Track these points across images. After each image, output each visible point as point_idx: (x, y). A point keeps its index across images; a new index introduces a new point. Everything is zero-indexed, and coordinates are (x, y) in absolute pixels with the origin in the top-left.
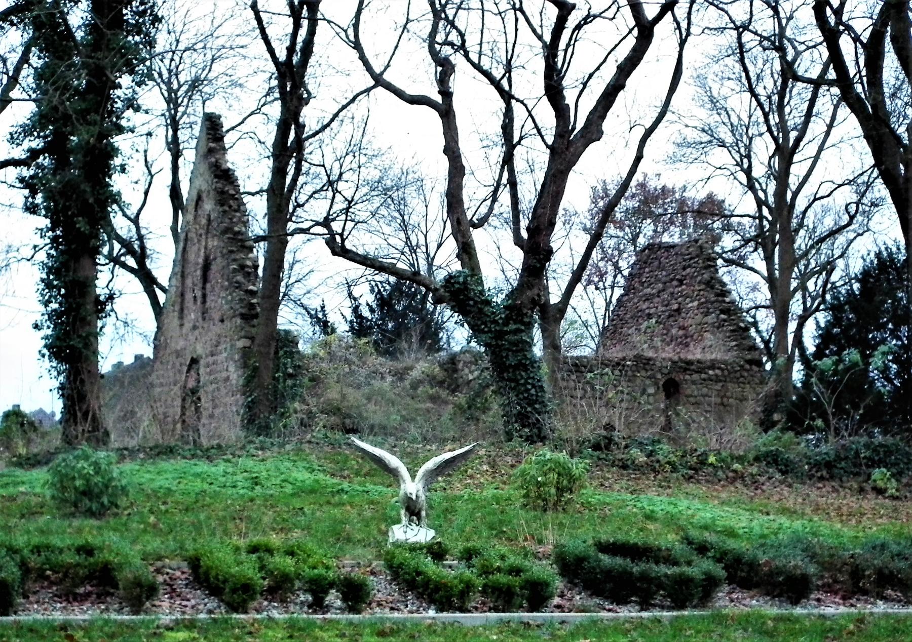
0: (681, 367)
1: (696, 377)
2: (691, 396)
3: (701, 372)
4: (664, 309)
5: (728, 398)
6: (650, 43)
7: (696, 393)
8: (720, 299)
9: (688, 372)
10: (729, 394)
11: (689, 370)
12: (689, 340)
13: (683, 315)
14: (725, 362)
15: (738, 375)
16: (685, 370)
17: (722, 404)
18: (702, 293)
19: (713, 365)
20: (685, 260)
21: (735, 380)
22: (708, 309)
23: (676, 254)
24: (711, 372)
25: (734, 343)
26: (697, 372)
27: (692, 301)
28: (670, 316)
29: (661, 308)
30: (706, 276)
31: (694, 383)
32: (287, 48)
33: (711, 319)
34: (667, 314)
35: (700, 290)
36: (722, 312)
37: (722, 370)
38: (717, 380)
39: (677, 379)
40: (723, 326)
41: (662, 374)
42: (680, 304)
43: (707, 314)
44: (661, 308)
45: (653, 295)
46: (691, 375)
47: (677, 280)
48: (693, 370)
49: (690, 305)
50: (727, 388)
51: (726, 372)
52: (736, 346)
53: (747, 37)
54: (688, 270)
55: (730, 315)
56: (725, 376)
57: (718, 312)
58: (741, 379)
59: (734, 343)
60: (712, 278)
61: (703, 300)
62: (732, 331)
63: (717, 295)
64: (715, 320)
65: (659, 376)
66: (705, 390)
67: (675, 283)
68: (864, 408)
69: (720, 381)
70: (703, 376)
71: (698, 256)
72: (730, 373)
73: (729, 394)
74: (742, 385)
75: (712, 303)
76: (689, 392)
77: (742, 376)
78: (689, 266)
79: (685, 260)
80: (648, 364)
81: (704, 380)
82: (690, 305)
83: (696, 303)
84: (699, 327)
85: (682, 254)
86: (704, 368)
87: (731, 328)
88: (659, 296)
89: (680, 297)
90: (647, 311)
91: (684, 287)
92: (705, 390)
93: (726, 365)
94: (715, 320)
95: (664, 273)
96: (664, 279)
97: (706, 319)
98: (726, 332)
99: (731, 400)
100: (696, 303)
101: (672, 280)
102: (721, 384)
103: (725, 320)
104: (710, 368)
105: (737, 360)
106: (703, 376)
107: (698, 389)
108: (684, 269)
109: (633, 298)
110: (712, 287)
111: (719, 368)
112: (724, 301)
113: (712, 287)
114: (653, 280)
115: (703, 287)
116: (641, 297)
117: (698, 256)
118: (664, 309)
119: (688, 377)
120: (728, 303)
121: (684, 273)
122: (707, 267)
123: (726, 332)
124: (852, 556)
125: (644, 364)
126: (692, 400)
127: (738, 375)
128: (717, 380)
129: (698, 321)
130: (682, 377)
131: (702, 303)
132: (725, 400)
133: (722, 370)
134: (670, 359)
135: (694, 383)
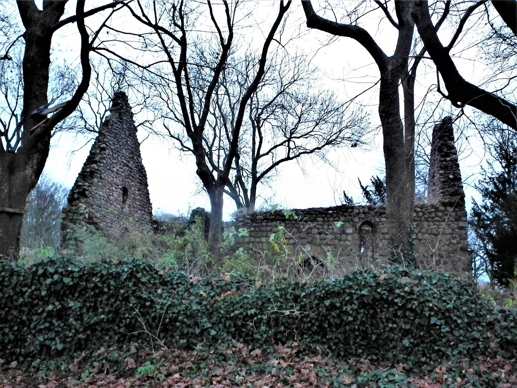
15: (433, 215)
21: (430, 219)
37: (417, 212)
39: (372, 221)
41: (359, 218)
56: (419, 217)
73: (423, 230)
74: (438, 223)
77: (437, 216)
80: (347, 211)
127: (433, 215)
130: (378, 220)
133: (417, 212)
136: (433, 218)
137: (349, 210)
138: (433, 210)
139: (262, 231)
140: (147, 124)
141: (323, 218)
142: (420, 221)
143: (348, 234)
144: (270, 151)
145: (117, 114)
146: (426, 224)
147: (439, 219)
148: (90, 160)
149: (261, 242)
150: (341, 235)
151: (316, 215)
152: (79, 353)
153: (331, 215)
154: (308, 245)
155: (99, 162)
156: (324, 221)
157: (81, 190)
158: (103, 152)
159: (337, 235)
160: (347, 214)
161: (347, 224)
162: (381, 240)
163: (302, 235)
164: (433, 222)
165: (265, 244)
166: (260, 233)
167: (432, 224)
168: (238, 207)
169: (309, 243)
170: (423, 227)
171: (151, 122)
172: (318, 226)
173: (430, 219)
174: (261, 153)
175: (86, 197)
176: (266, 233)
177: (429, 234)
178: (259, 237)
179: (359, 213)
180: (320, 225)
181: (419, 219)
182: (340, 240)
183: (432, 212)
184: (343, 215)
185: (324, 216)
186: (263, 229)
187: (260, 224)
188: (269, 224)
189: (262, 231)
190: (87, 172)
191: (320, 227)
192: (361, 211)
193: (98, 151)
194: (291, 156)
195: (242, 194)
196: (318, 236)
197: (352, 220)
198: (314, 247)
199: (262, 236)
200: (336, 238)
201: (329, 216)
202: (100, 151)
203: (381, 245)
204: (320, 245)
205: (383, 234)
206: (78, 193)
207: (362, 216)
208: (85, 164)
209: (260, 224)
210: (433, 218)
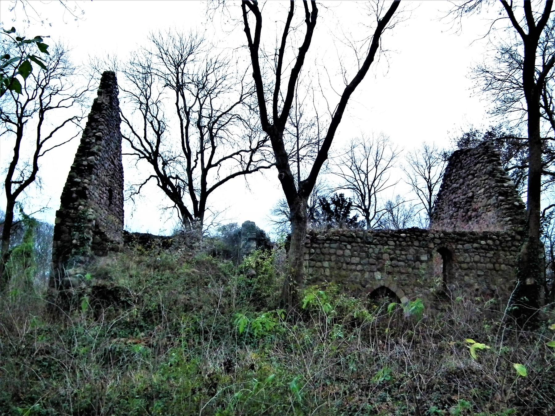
0: (453, 238)
1: (467, 246)
2: (464, 262)
4: (463, 197)
5: (500, 264)
6: (362, 79)
7: (468, 260)
8: (499, 184)
9: (460, 242)
10: (501, 260)
11: (461, 240)
12: (479, 218)
13: (475, 200)
14: (498, 234)
15: (509, 244)
16: (457, 240)
17: (494, 269)
18: (486, 181)
19: (485, 236)
20: (475, 158)
21: (507, 249)
22: (491, 193)
23: (471, 155)
24: (483, 242)
25: (509, 218)
26: (469, 242)
27: (480, 189)
28: (467, 202)
29: (462, 197)
30: (489, 168)
31: (466, 251)
32: (300, 49)
33: (492, 201)
34: (465, 200)
35: (485, 180)
36: (500, 194)
37: (494, 240)
38: (488, 248)
39: (449, 248)
40: (501, 205)
41: (435, 244)
42: (473, 192)
43: (489, 197)
44: (462, 197)
45: (457, 188)
46: (463, 245)
47: (471, 174)
48: (465, 240)
49: (479, 192)
50: (499, 256)
51: (498, 242)
52: (509, 220)
53: (254, 146)
54: (478, 166)
55: (507, 197)
56: (496, 246)
57: (497, 195)
58: (513, 248)
59: (509, 218)
60: (494, 169)
61: (487, 187)
62: (507, 209)
63: (497, 181)
64: (495, 201)
66: (477, 258)
67: (470, 177)
69: (492, 250)
71: (484, 154)
72: (501, 243)
73: (501, 260)
74: (514, 253)
75: (493, 188)
76: (461, 259)
77: (513, 245)
78: (479, 163)
79: (475, 158)
80: (421, 235)
81: (476, 248)
82: (479, 192)
83: (483, 190)
84: (485, 208)
85: (474, 155)
87: (507, 206)
88: (461, 189)
89: (474, 186)
90: (454, 200)
91: (476, 179)
92: (477, 258)
94: (495, 201)
95: (464, 171)
96: (464, 175)
97: (489, 202)
98: (503, 210)
99: (503, 266)
100: (483, 190)
101: (468, 175)
102: (493, 252)
103: (502, 201)
104: (482, 239)
105: (509, 232)
106: (475, 245)
107: (470, 257)
108: (475, 165)
109: (446, 192)
110: (494, 176)
111: (491, 239)
112: (503, 186)
113: (494, 176)
114: (457, 177)
115: (487, 176)
116: (450, 191)
117: (484, 154)
118: (463, 197)
120: (507, 187)
121: (475, 169)
122: (490, 162)
123: (503, 210)
126: (465, 266)
127: (509, 244)
128: (488, 248)
129: (484, 204)
130: (454, 247)
131: (487, 189)
132: (497, 265)
133: (494, 240)
135: (466, 251)
136: (510, 247)
137: (424, 234)
138: (510, 239)
139: (323, 254)
140: (75, 121)
141: (395, 241)
143: (422, 262)
144: (218, 163)
145: (108, 98)
146: (502, 253)
147: (516, 249)
148: (84, 150)
149: (323, 267)
150: (415, 262)
151: (387, 237)
153: (404, 238)
155: (97, 154)
156: (396, 245)
157: (80, 188)
158: (98, 142)
159: (410, 262)
161: (422, 250)
162: (457, 270)
163: (371, 260)
164: (510, 251)
166: (322, 257)
167: (508, 254)
168: (185, 222)
169: (378, 270)
170: (499, 257)
171: (79, 119)
172: (389, 250)
173: (507, 249)
174: (213, 163)
175: (86, 198)
177: (506, 265)
178: (320, 261)
179: (435, 238)
181: (495, 248)
182: (413, 268)
183: (508, 241)
184: (417, 239)
185: (395, 239)
186: (325, 251)
188: (333, 245)
189: (323, 254)
190: (84, 166)
191: (392, 252)
192: (437, 235)
193: (94, 141)
194: (249, 169)
197: (427, 246)
199: (324, 260)
202: (96, 141)
206: (77, 192)
207: (438, 241)
208: (76, 155)
209: (321, 246)
210: (510, 247)
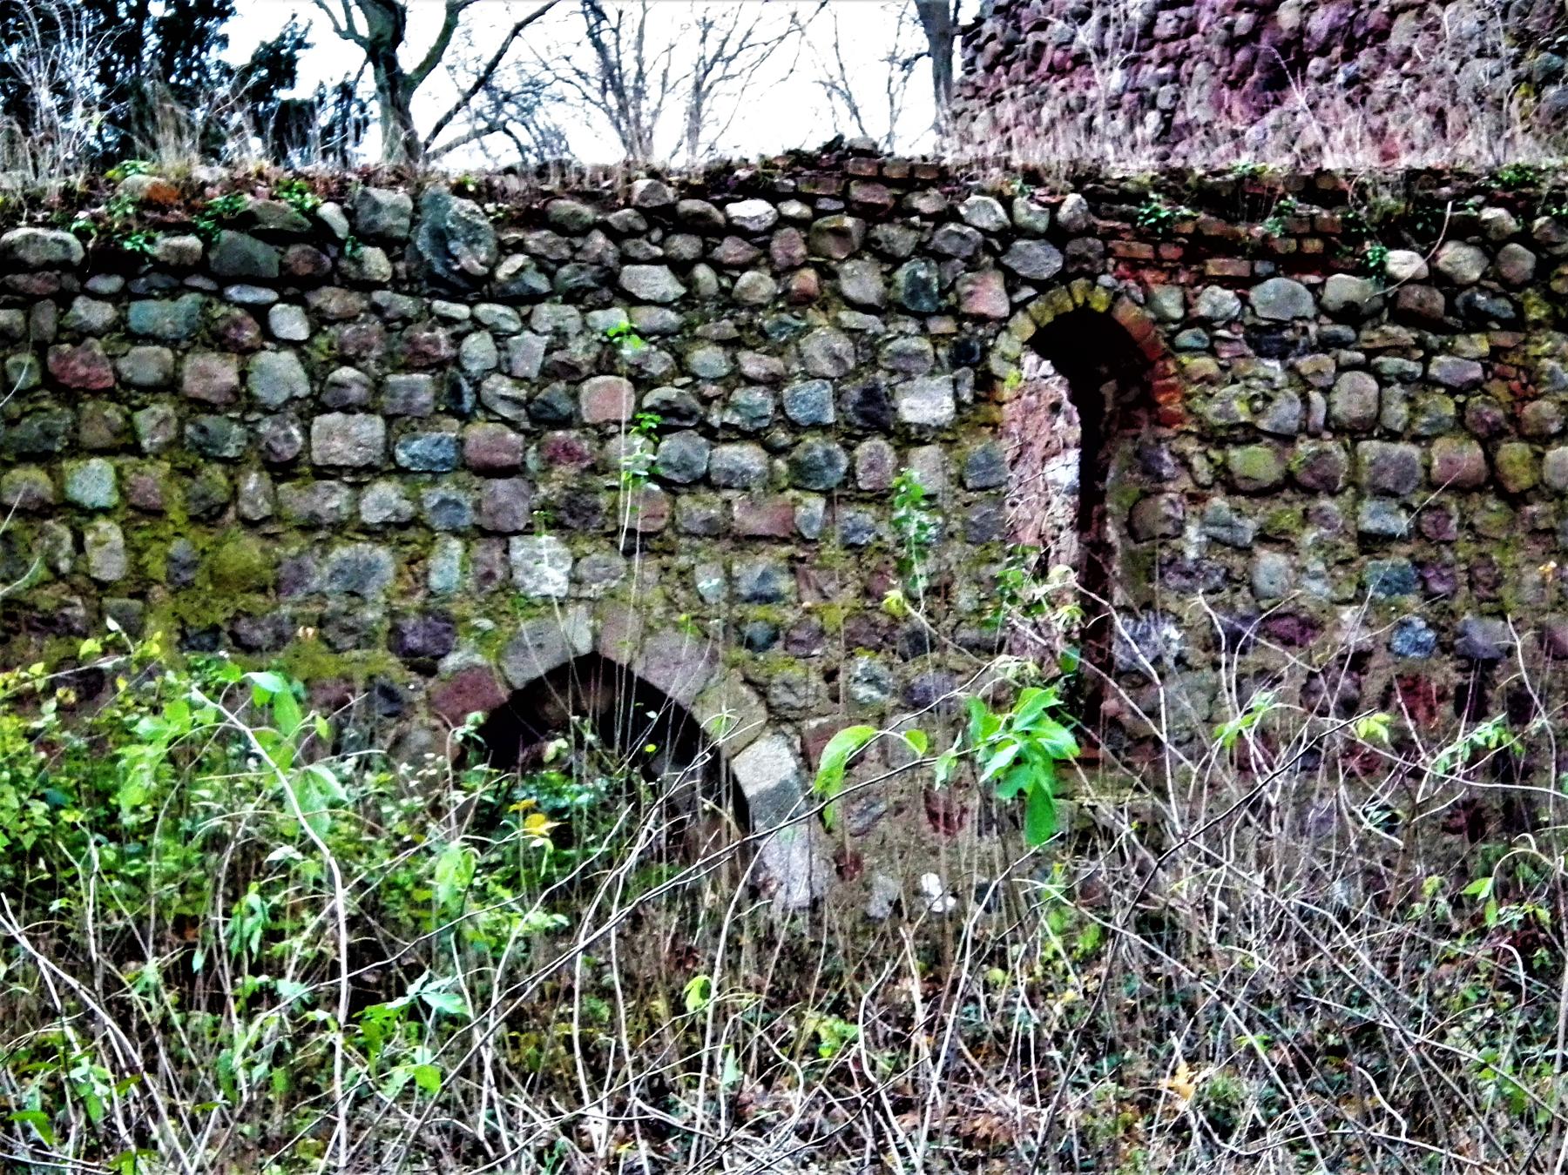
0: (1163, 232)
1: (1276, 295)
2: (1251, 434)
3: (1325, 265)
11: (1229, 247)
12: (1365, 59)
16: (1199, 248)
19: (1423, 209)
24: (1404, 263)
26: (1292, 265)
31: (1268, 338)
37: (1489, 242)
39: (1128, 313)
41: (1012, 281)
48: (1264, 250)
50: (1530, 371)
56: (1509, 287)
65: (990, 297)
68: (155, 30)
69: (1477, 321)
70: (1343, 287)
80: (900, 212)
81: (1350, 314)
86: (1352, 234)
92: (1354, 395)
93: (1523, 207)
104: (1393, 233)
106: (1343, 287)
111: (1466, 230)
119: (1218, 300)
124: (1093, 808)
125: (871, 215)
126: (1255, 462)
128: (1448, 312)
130: (1171, 303)
132: (1513, 452)
134: (1085, 179)
135: (1268, 338)
137: (926, 203)
139: (70, 394)
141: (681, 269)
142: (1517, 323)
143: (907, 438)
152: (127, 346)
154: (547, 542)
156: (689, 300)
159: (815, 446)
160: (894, 235)
161: (907, 338)
165: (108, 531)
176: (113, 412)
178: (44, 458)
179: (1012, 232)
180: (661, 336)
181: (1502, 307)
185: (686, 246)
187: (46, 318)
189: (70, 394)
191: (659, 363)
195: (246, 242)
196: (632, 452)
198: (599, 556)
199: (78, 450)
200: (803, 475)
201: (730, 249)
203: (1193, 540)
204: (647, 543)
205: (1211, 437)
